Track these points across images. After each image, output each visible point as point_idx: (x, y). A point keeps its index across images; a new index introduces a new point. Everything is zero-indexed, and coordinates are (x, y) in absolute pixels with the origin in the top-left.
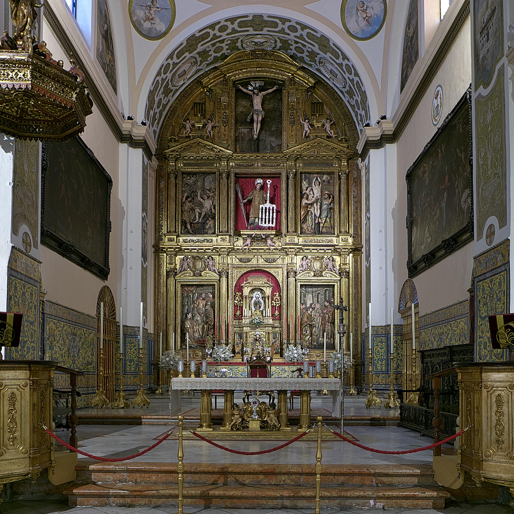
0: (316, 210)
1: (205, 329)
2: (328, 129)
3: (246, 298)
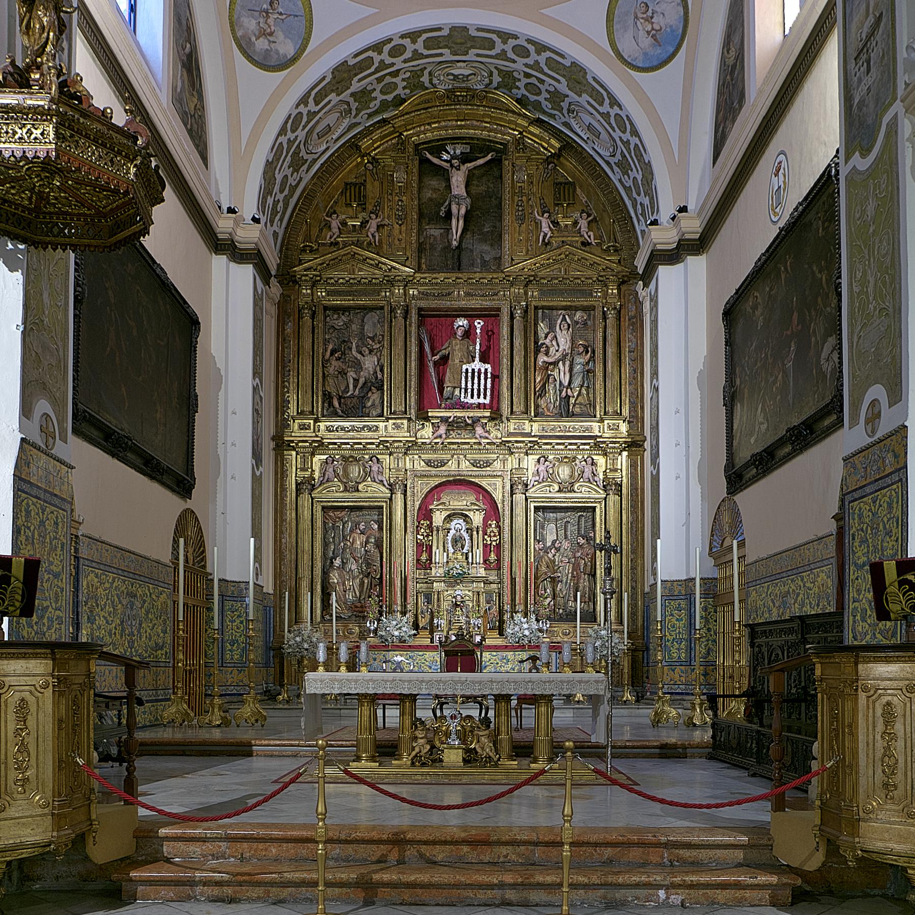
1: (366, 585)
2: (584, 229)
3: (438, 531)
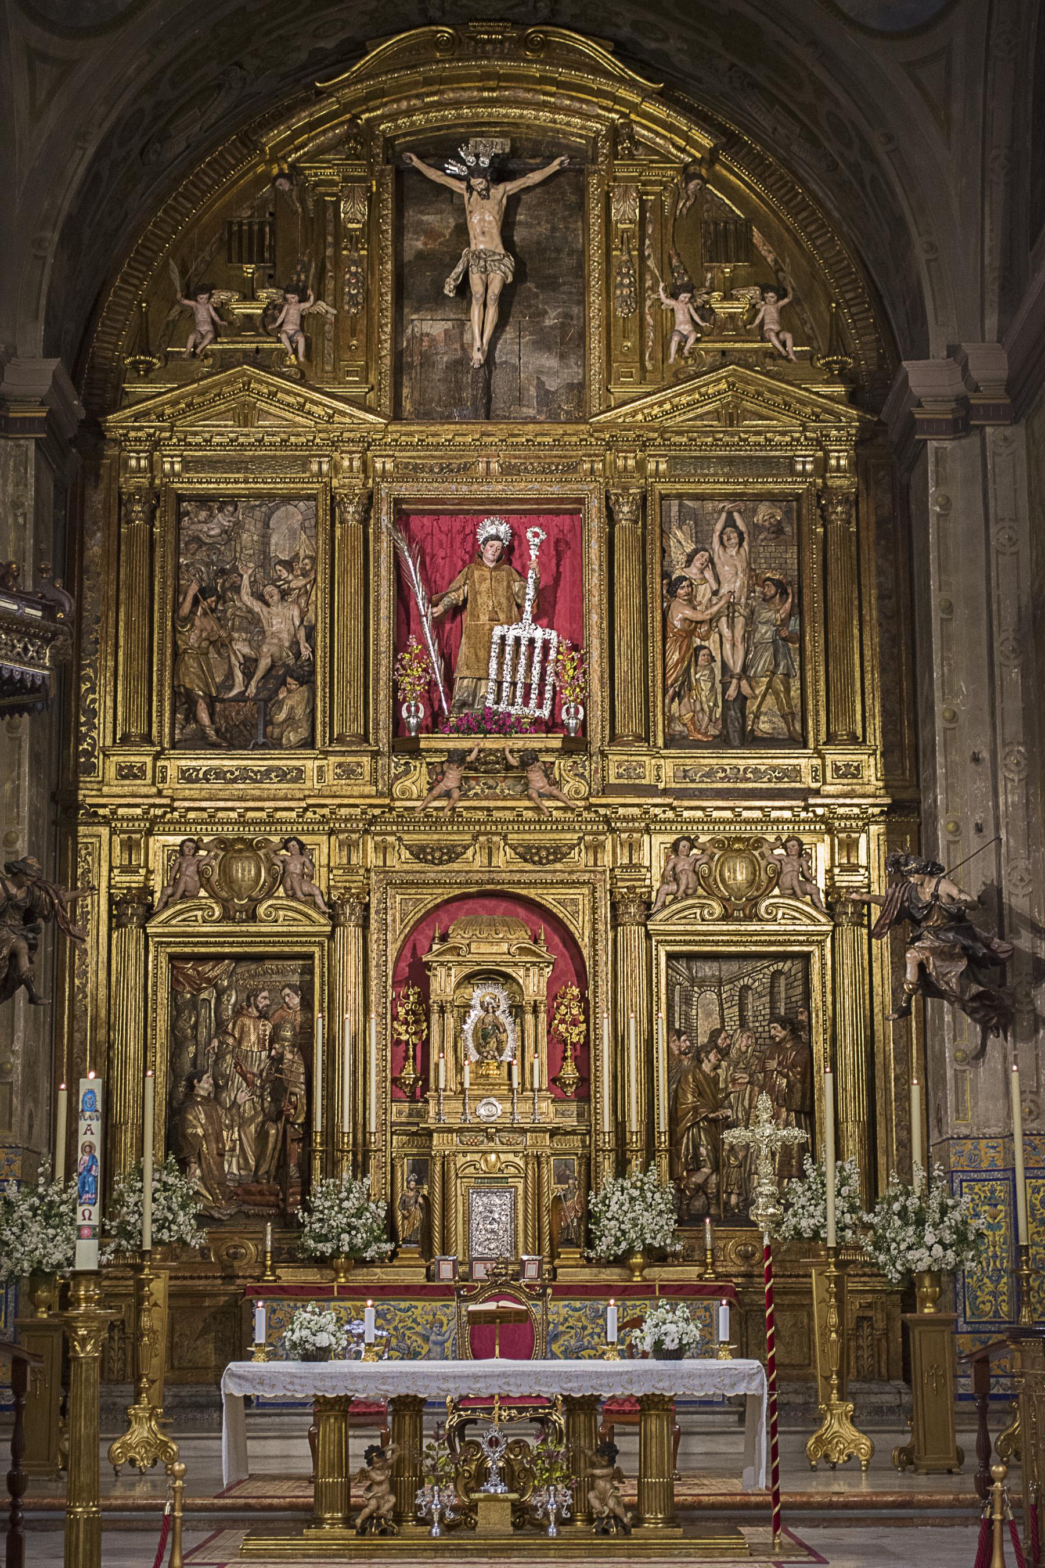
0: (726, 646)
1: (271, 1140)
2: (772, 326)
3: (442, 1011)
